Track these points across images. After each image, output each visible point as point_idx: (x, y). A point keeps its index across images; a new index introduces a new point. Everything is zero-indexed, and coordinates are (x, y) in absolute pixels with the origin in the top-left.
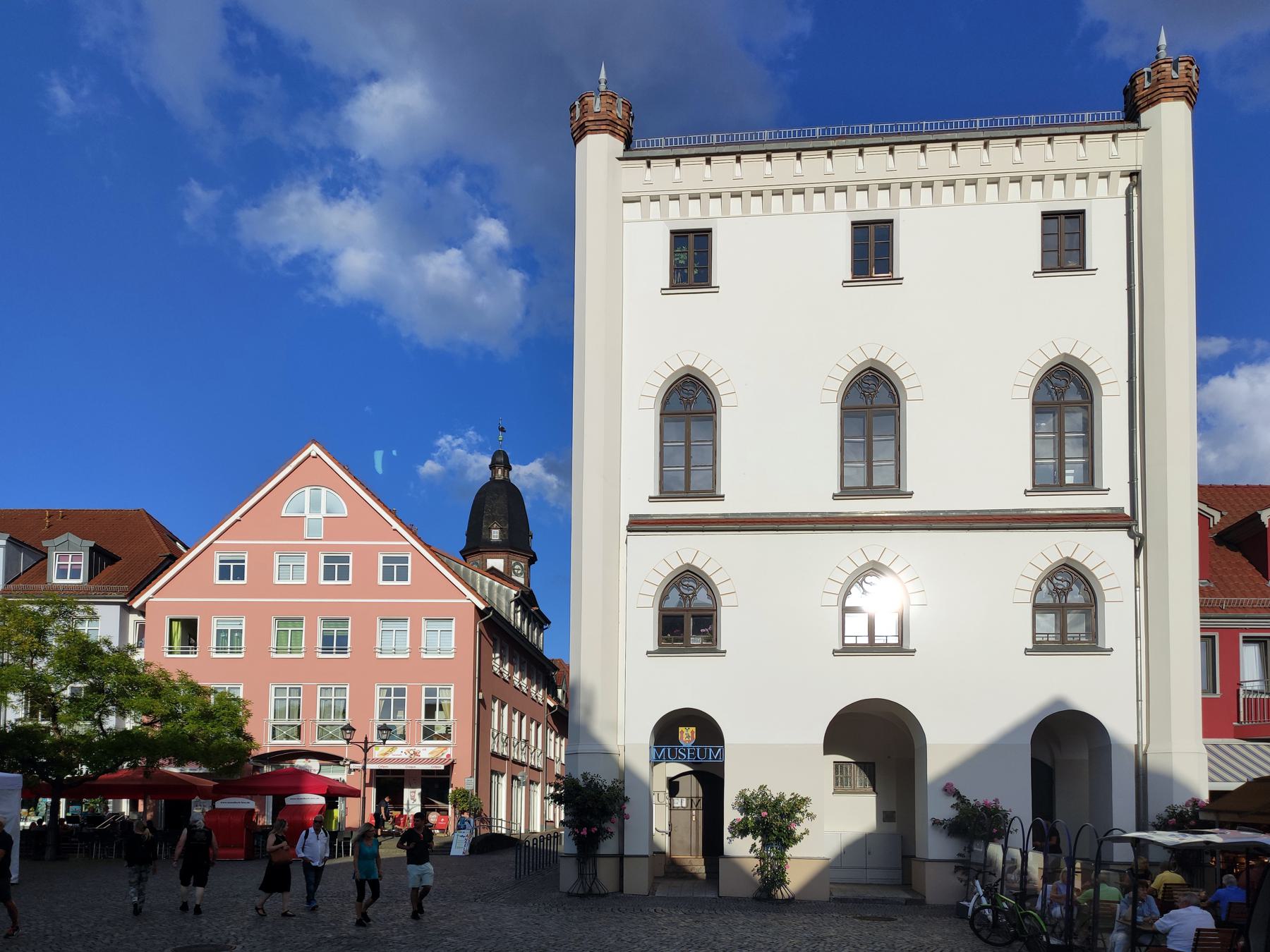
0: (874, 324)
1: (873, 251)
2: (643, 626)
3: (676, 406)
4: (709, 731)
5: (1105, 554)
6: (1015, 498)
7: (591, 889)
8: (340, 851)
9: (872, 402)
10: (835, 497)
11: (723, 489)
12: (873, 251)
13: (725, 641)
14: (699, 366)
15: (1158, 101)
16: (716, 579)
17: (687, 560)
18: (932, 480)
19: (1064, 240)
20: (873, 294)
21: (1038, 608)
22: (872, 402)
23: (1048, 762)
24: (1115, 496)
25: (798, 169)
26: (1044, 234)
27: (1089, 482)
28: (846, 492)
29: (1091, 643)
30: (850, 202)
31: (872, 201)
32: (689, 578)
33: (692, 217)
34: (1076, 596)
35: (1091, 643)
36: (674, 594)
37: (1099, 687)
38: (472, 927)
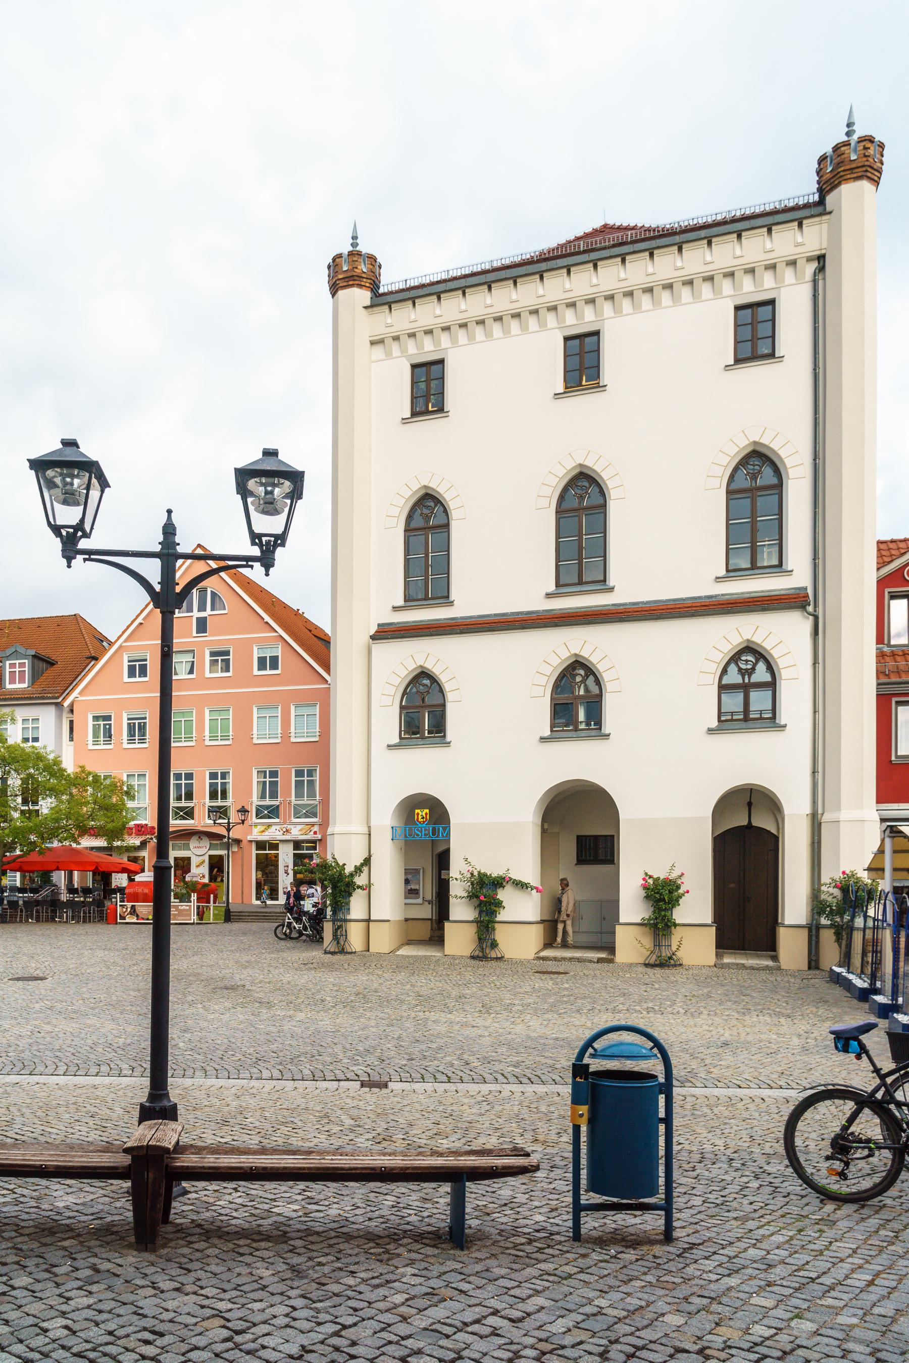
0: (585, 432)
1: (583, 362)
2: (388, 723)
3: (418, 522)
4: (438, 813)
5: (785, 637)
6: (537, 603)
7: (343, 949)
8: (21, 917)
9: (582, 503)
10: (549, 596)
11: (611, 582)
12: (583, 362)
13: (608, 725)
14: (765, 441)
15: (839, 184)
16: (775, 653)
17: (420, 662)
18: (633, 573)
19: (755, 332)
20: (584, 404)
21: (723, 688)
22: (582, 503)
23: (774, 831)
24: (798, 576)
25: (769, 245)
26: (737, 326)
27: (779, 567)
28: (732, 572)
29: (771, 721)
30: (404, 350)
31: (420, 346)
32: (751, 650)
33: (427, 350)
34: (761, 674)
35: (771, 721)
36: (733, 668)
37: (775, 762)
38: (408, 987)
